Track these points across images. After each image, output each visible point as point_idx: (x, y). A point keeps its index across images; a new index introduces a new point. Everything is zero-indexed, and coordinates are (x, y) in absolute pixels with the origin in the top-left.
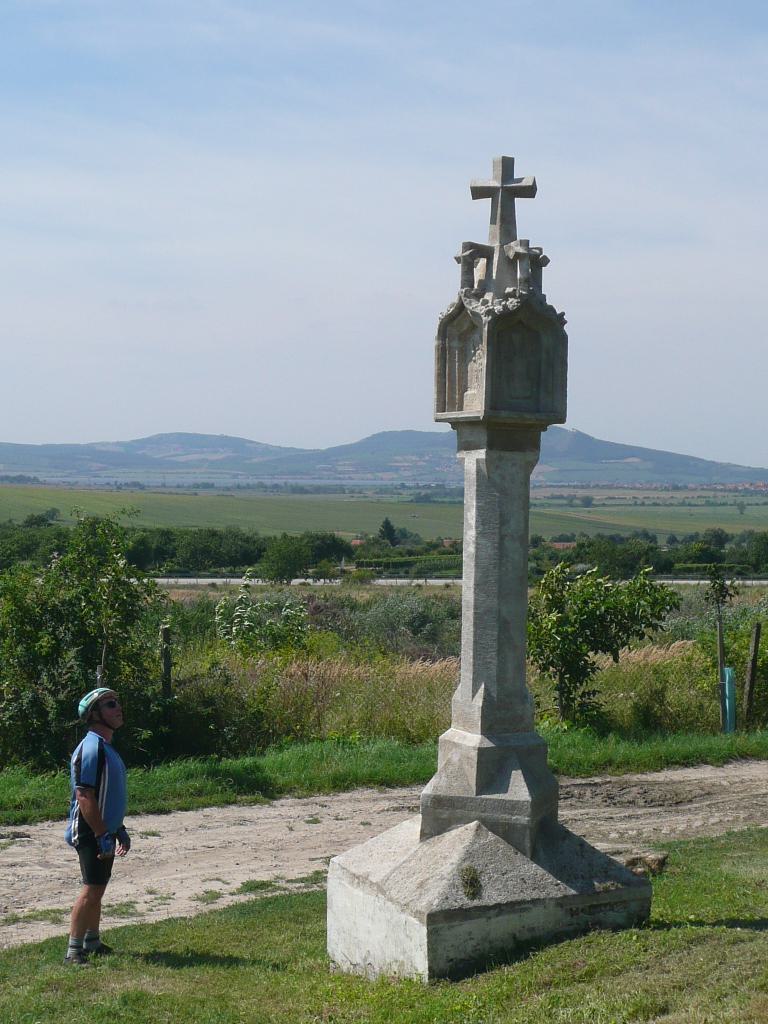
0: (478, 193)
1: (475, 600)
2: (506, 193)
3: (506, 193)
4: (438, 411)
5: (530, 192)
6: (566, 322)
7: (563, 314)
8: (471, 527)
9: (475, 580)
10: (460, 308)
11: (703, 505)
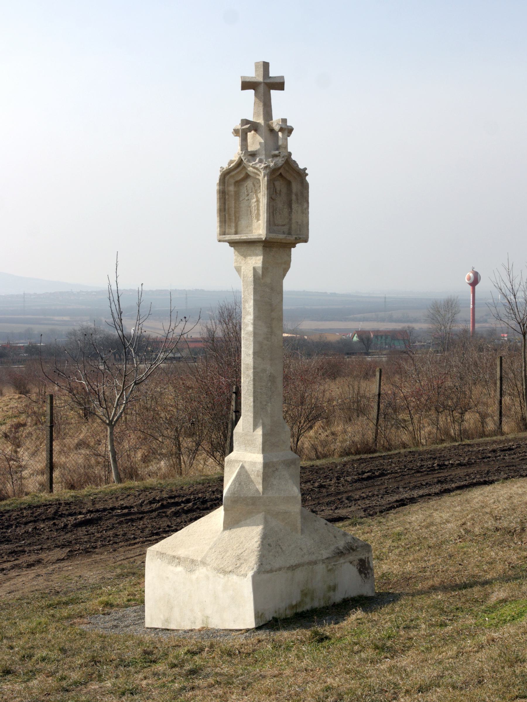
0: (246, 85)
1: (254, 362)
2: (265, 86)
3: (265, 86)
4: (220, 235)
5: (280, 85)
6: (307, 175)
7: (305, 169)
8: (248, 313)
9: (254, 349)
10: (240, 163)
11: (63, 559)
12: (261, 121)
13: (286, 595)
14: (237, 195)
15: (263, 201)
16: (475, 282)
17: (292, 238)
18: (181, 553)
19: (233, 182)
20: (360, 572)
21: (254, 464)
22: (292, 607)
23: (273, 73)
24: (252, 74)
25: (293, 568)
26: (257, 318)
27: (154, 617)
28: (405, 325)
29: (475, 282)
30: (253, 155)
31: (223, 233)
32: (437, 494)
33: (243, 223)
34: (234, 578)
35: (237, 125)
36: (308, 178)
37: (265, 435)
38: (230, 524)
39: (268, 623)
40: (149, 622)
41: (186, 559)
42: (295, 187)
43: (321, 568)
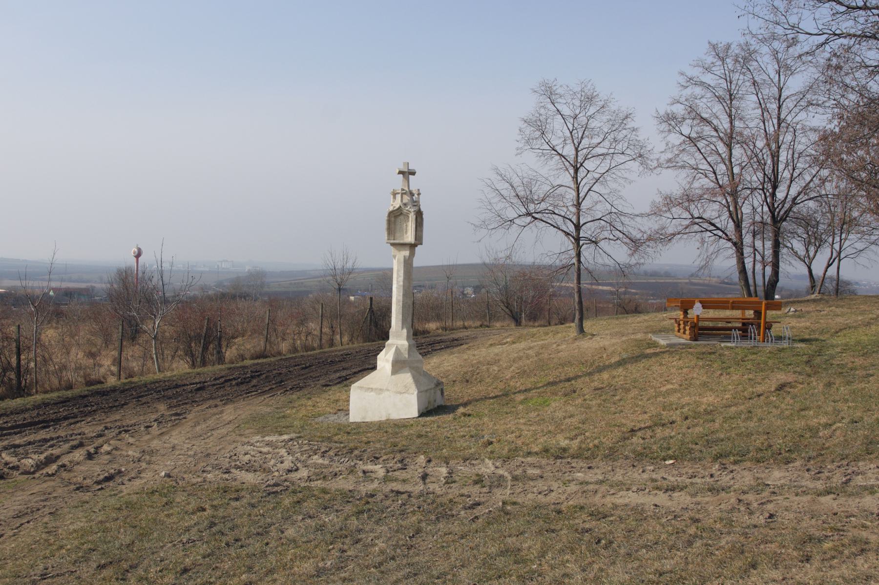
0: (400, 172)
12: (406, 189)
14: (395, 222)
16: (138, 256)
19: (395, 217)
21: (403, 345)
28: (89, 284)
29: (138, 256)
30: (405, 205)
32: (27, 410)
33: (398, 235)
39: (422, 415)
40: (352, 420)
41: (376, 389)
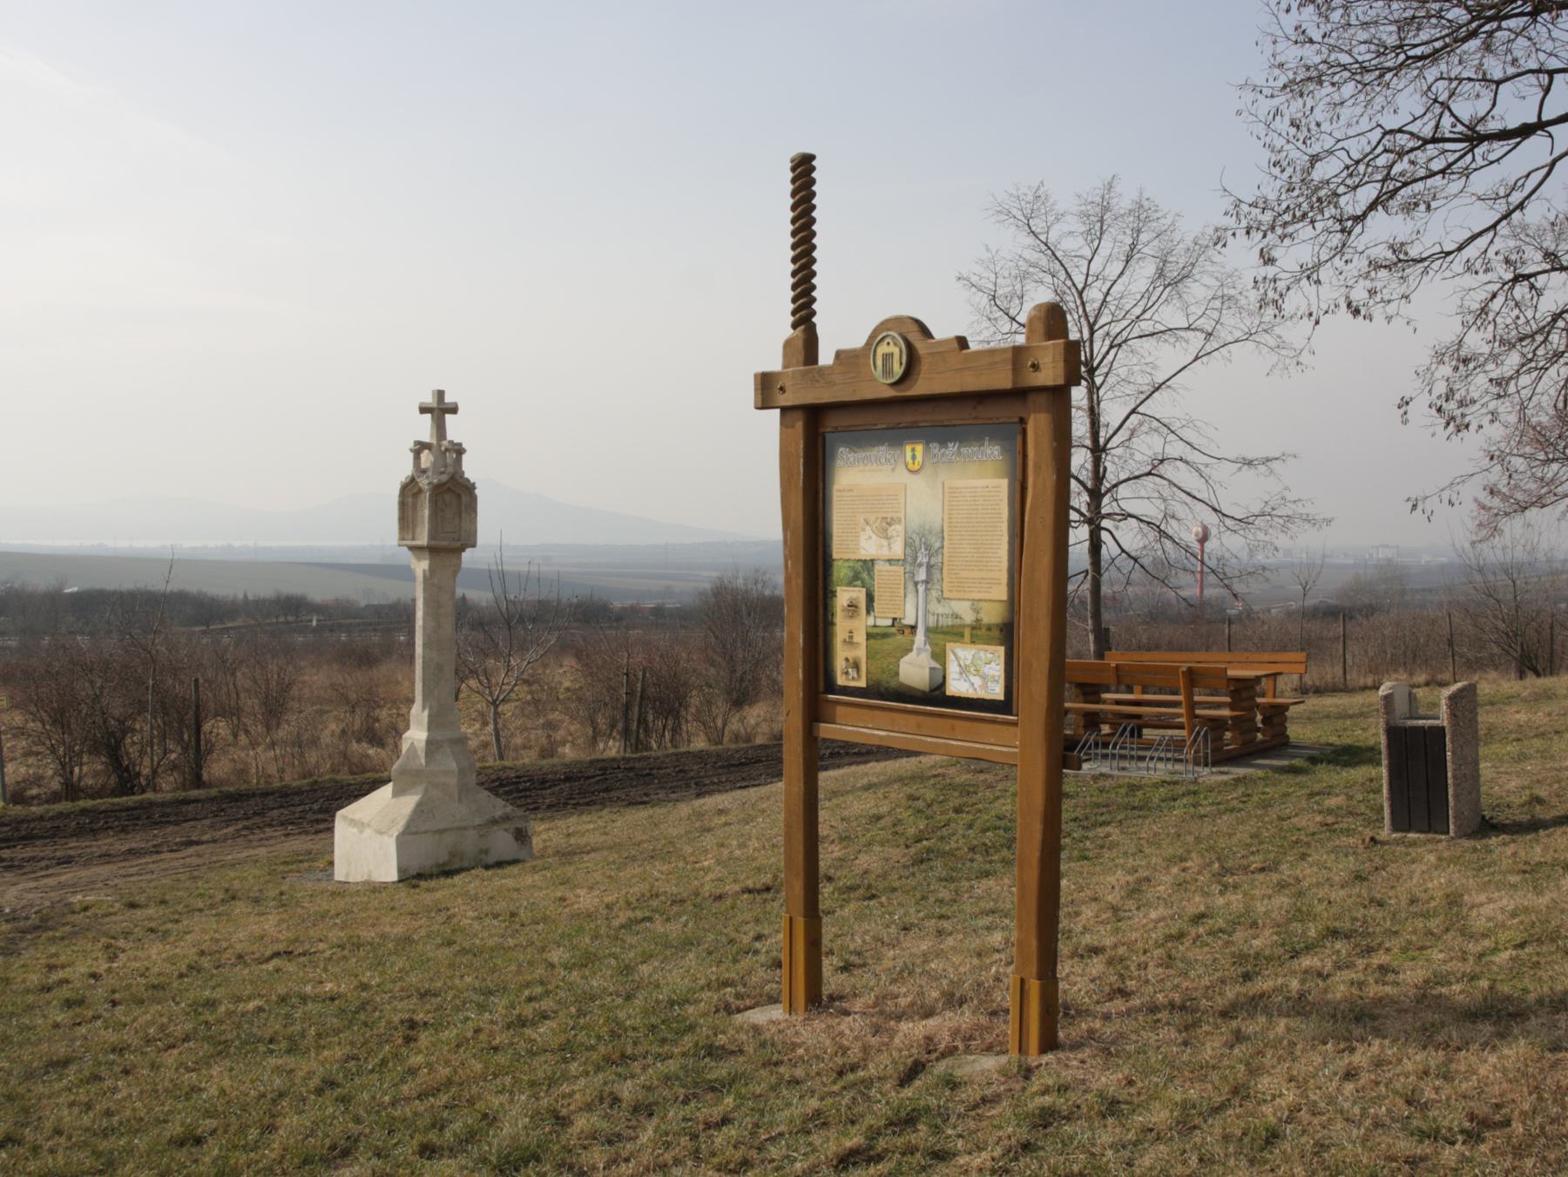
0: (424, 410)
2: (440, 410)
12: (434, 442)
13: (429, 852)
15: (427, 512)
17: (458, 544)
18: (357, 816)
20: (516, 839)
22: (438, 865)
23: (448, 399)
24: (429, 400)
25: (441, 832)
26: (426, 614)
27: (340, 873)
30: (424, 471)
31: (402, 539)
34: (385, 838)
35: (411, 445)
36: (477, 492)
37: (430, 716)
38: (397, 793)
39: (411, 878)
42: (465, 499)
43: (471, 835)
